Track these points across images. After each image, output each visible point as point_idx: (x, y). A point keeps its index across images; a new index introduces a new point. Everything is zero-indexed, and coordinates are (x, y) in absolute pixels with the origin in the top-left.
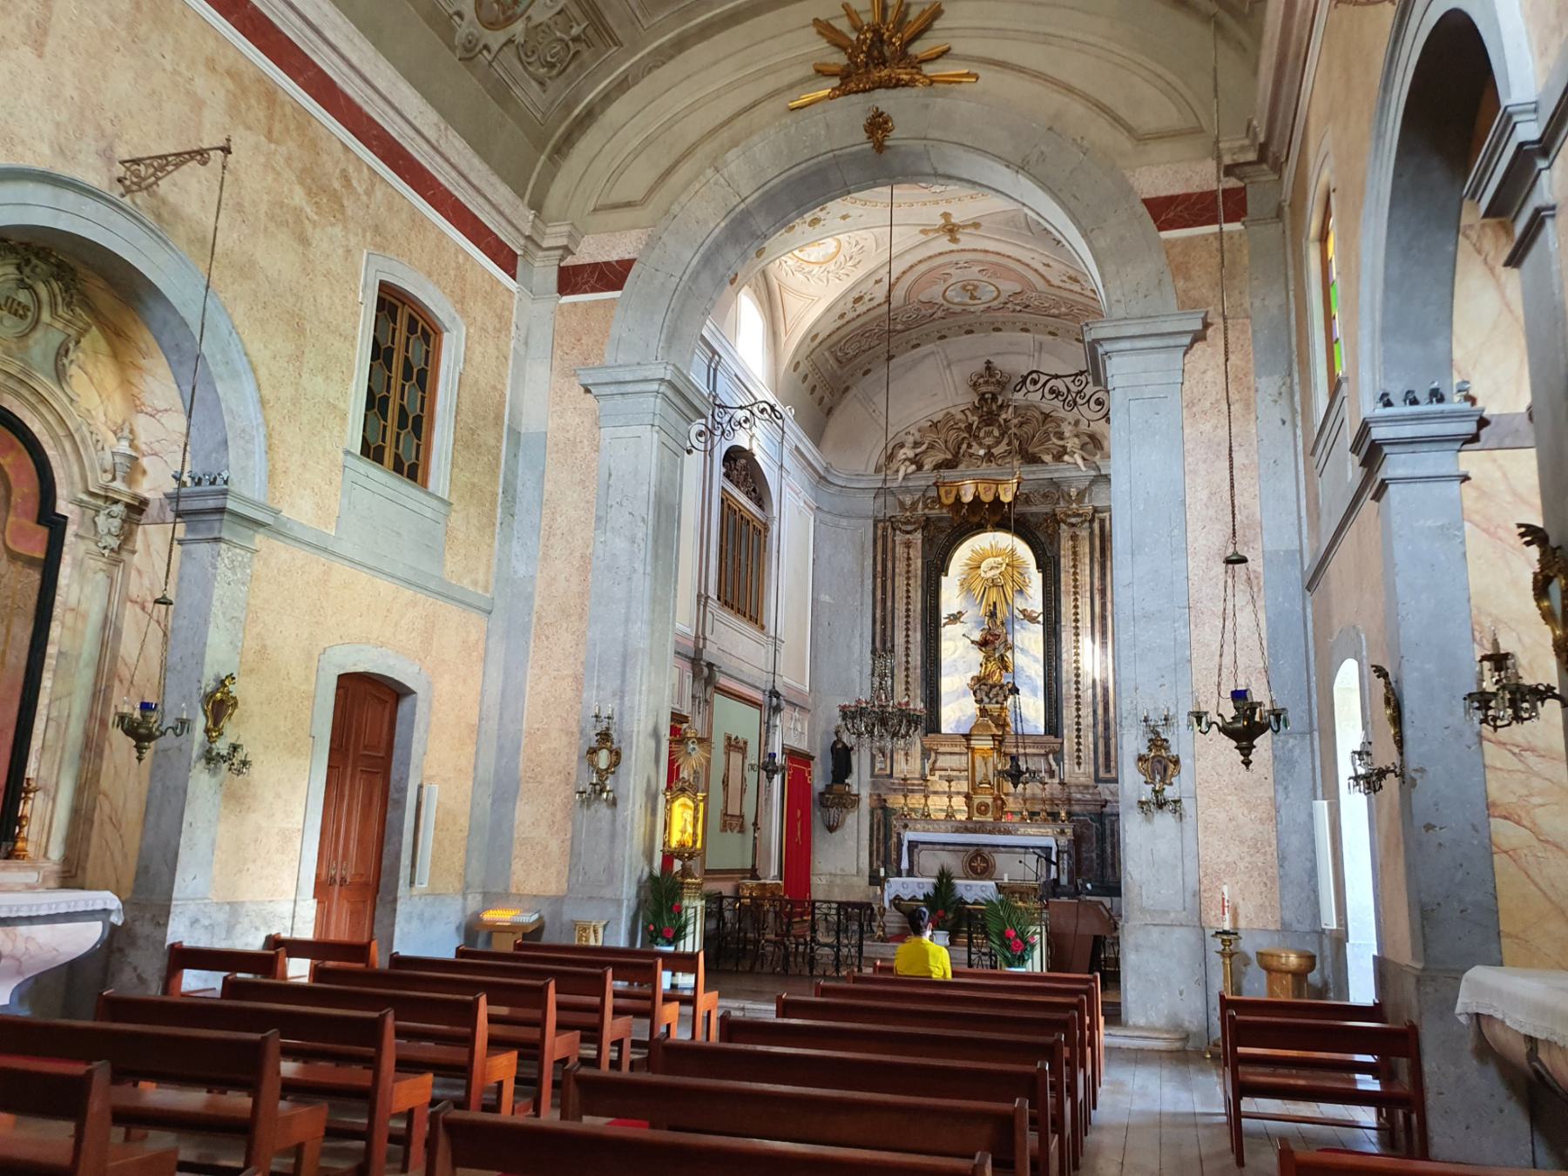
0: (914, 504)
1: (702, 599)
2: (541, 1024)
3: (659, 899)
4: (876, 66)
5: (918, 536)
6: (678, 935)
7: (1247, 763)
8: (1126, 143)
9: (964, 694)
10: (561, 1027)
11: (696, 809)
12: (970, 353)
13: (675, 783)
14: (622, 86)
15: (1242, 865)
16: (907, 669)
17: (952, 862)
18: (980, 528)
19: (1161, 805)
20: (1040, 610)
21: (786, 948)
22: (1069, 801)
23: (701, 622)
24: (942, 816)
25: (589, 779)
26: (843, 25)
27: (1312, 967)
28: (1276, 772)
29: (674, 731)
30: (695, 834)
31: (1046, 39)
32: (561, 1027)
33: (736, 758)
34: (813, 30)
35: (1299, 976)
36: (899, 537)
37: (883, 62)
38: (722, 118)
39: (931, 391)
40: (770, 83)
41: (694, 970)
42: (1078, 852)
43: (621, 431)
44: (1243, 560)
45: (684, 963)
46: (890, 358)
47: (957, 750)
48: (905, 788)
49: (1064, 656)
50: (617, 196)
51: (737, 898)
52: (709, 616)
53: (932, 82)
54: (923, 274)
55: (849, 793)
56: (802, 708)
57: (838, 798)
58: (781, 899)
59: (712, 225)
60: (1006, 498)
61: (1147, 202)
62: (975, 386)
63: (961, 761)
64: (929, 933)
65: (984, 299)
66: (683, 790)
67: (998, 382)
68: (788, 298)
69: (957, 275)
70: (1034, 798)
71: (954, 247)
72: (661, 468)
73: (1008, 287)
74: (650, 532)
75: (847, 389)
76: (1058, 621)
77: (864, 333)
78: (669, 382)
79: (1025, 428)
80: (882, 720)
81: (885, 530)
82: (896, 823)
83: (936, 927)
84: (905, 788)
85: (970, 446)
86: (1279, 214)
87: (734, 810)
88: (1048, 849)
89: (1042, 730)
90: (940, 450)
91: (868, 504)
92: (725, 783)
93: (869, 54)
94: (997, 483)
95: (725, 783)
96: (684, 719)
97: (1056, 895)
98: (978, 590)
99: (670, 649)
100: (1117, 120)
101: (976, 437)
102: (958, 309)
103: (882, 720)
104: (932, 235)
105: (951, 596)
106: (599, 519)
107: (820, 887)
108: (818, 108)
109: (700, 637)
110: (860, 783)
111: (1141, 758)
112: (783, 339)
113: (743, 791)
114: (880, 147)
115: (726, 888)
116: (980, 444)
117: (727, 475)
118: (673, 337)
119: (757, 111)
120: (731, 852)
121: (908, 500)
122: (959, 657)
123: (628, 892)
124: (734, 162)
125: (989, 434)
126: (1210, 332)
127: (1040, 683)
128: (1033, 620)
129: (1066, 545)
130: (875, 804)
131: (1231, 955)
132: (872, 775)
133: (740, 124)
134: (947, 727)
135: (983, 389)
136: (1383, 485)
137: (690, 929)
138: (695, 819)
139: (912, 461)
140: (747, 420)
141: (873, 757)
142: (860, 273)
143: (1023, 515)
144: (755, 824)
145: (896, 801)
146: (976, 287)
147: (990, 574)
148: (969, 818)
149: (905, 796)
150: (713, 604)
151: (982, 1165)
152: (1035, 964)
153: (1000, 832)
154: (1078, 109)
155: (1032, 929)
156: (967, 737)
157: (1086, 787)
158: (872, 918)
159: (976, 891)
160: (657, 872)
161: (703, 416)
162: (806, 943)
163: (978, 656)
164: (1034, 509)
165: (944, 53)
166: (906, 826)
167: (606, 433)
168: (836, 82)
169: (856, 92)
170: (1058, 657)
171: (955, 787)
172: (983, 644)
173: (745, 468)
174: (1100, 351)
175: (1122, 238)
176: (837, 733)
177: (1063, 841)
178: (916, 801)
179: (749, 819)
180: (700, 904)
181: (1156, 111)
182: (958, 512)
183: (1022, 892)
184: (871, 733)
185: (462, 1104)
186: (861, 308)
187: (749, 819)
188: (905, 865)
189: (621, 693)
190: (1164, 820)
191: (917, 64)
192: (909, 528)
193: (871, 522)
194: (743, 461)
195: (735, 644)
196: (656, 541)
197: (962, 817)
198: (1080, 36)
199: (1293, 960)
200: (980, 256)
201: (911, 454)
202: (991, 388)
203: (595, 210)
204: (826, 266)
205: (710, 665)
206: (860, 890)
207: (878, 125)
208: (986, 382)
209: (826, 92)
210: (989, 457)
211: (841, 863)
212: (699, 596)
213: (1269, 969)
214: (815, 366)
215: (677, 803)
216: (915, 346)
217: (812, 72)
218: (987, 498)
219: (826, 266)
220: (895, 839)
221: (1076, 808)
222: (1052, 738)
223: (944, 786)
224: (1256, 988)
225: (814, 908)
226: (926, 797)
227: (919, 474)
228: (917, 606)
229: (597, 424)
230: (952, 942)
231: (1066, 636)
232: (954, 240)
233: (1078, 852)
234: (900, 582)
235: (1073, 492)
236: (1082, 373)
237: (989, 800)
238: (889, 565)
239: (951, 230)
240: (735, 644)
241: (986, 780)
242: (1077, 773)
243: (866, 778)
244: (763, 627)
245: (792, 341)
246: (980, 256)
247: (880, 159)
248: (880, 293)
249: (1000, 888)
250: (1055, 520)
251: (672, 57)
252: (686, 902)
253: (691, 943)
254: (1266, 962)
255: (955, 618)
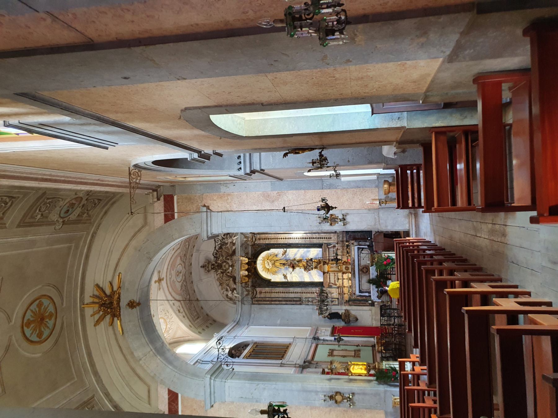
0: (248, 291)
1: (282, 365)
2: (424, 408)
3: (383, 377)
4: (112, 305)
5: (258, 289)
6: (394, 369)
7: (336, 208)
8: (147, 228)
9: (310, 274)
10: (424, 402)
11: (354, 364)
12: (197, 271)
13: (347, 372)
14: (107, 395)
15: (360, 198)
16: (302, 293)
17: (365, 279)
18: (256, 269)
19: (344, 219)
20: (282, 249)
21: (396, 334)
22: (342, 241)
23: (289, 365)
24: (350, 282)
25: (346, 403)
26: (97, 317)
27: (387, 181)
28: (333, 188)
29: (328, 373)
30: (362, 365)
31: (111, 252)
32: (424, 402)
33: (335, 353)
34: (97, 327)
35: (390, 184)
36: (258, 296)
37: (111, 303)
38: (123, 358)
39: (209, 286)
40: (113, 342)
41: (404, 362)
42: (358, 239)
43: (227, 394)
44: (284, 208)
45: (402, 365)
46: (197, 300)
47: (328, 276)
48: (342, 294)
49: (297, 242)
50: (145, 395)
51: (381, 352)
52: (288, 363)
53: (120, 287)
54: (173, 289)
55: (345, 313)
56: (317, 330)
57: (347, 317)
58: (381, 336)
59: (159, 361)
60: (246, 260)
61: (166, 222)
62: (209, 271)
63: (332, 275)
64: (386, 288)
65: (181, 269)
66: (348, 369)
67: (208, 263)
68: (177, 336)
69: (174, 278)
70: (342, 252)
71: (165, 279)
72: (239, 379)
73: (179, 261)
74: (261, 383)
75: (207, 315)
76: (286, 244)
77: (189, 309)
78: (211, 376)
79: (223, 254)
80: (323, 300)
81: (256, 301)
82: (353, 297)
83: (386, 285)
84: (342, 294)
85: (228, 272)
86: (173, 186)
87: (353, 354)
88: (359, 248)
89: (321, 249)
90: (229, 282)
91: (246, 307)
92: (344, 356)
93: (108, 308)
94: (242, 263)
95: (344, 356)
96: (324, 370)
97: (372, 246)
98: (275, 269)
99: (301, 375)
100: (139, 231)
101: (226, 270)
102: (184, 277)
103: (323, 300)
104: (161, 287)
105: (278, 278)
106: (257, 401)
107: (376, 323)
108: (123, 325)
109: (295, 366)
110: (341, 309)
111: (331, 225)
112: (190, 338)
113: (346, 350)
114: (139, 304)
115: (379, 356)
116: (228, 269)
117: (238, 357)
118: (195, 375)
119: (121, 345)
120: (367, 353)
121: (246, 293)
122: (297, 275)
123: (382, 388)
124: (138, 354)
125: (225, 266)
126: (206, 205)
127: (306, 249)
128: (286, 252)
129: (262, 242)
130: (348, 304)
131: (386, 201)
132: (338, 305)
133: (125, 351)
134: (321, 280)
135: (210, 268)
136: (262, 170)
137: (392, 366)
138: (357, 365)
139: (233, 292)
140: (223, 349)
141: (334, 305)
142: (171, 311)
143: (252, 255)
144: (357, 346)
145: (346, 297)
146: (178, 272)
147: (271, 265)
148: (350, 273)
149: (345, 294)
150: (284, 361)
151: (433, 279)
152: (393, 255)
153: (354, 263)
154: (134, 243)
155: (383, 256)
156: (324, 273)
157: (338, 236)
158: (385, 305)
159: (373, 273)
160: (375, 378)
161: (221, 364)
162: (395, 328)
163: (297, 269)
164: (250, 252)
165: (111, 284)
166: (354, 294)
167: (227, 399)
168: (116, 319)
169: (120, 312)
170: (297, 244)
171: (340, 277)
172: (293, 267)
173: (235, 351)
174: (210, 236)
175: (176, 229)
176: (325, 317)
177: (356, 244)
178: (346, 290)
179: (355, 348)
180: (384, 363)
181: (138, 220)
182: (251, 276)
183: (373, 259)
184: (327, 305)
185: (435, 409)
186: (182, 310)
187: (355, 348)
188: (367, 294)
189: (317, 392)
190: (348, 218)
191: (113, 292)
192: (255, 292)
193: (253, 306)
194: (233, 351)
195: (297, 353)
196: (264, 381)
197: (350, 275)
198: (111, 242)
199: (386, 186)
200: (169, 270)
201: (230, 292)
202: (210, 266)
203: (150, 404)
204: (169, 322)
205: (305, 362)
206: (376, 310)
207: (132, 305)
208: (208, 267)
209: (119, 321)
210: (232, 266)
211: (368, 316)
212: (281, 366)
213: (389, 192)
214: (200, 326)
215: (352, 371)
216: (195, 292)
217: (111, 327)
218: (247, 267)
219: (169, 322)
220: (359, 298)
221: (345, 239)
222: (323, 246)
223: (340, 281)
224: (394, 195)
225: (383, 325)
226: (344, 287)
227: (237, 289)
228: (281, 289)
229: (224, 402)
230: (390, 279)
231: (291, 241)
232: (163, 279)
233: (358, 239)
234: (273, 295)
235: (245, 239)
236: (215, 240)
237: (344, 266)
238: (267, 299)
239: (160, 280)
240: (297, 353)
241: (337, 267)
242: (334, 239)
243: (339, 307)
244: (290, 344)
245: (192, 334)
246: (169, 270)
247: (141, 305)
248: (177, 304)
249: (372, 265)
250: (254, 245)
251: (100, 377)
252: (384, 367)
253: (396, 365)
254: (387, 193)
255: (285, 277)
